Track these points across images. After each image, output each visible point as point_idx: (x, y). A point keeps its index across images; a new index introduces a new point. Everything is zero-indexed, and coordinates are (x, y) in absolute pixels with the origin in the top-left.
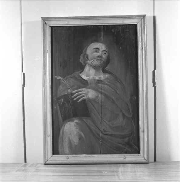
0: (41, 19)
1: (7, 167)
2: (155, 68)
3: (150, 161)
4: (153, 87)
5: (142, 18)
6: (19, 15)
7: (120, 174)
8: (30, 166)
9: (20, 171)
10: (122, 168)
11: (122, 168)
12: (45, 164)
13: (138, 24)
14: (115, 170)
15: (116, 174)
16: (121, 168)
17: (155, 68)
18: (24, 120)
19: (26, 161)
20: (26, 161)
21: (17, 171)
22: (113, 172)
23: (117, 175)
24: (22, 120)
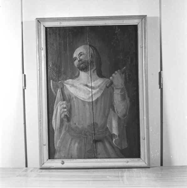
0: (34, 19)
1: (9, 172)
2: (160, 74)
3: (152, 165)
4: (160, 89)
5: (142, 19)
6: (20, 16)
7: (125, 178)
8: (31, 171)
9: (20, 176)
10: (127, 173)
11: (127, 173)
12: (40, 169)
13: (139, 24)
14: (120, 175)
15: (120, 179)
16: (126, 173)
17: (161, 70)
18: (25, 123)
19: (27, 166)
20: (27, 166)
21: (17, 176)
22: (118, 177)
23: (122, 180)
24: (23, 123)
